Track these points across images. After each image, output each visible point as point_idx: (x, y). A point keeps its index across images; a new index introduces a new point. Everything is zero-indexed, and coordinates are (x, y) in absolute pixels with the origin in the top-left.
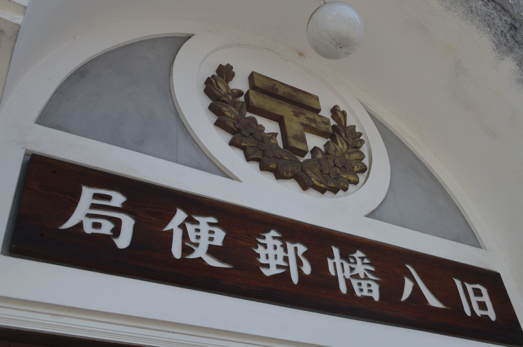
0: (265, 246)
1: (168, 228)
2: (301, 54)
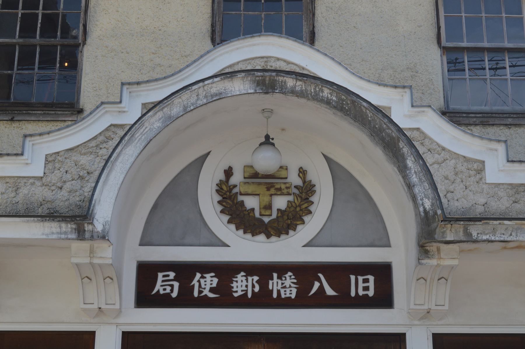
0: (237, 282)
1: (192, 284)
2: (283, 130)
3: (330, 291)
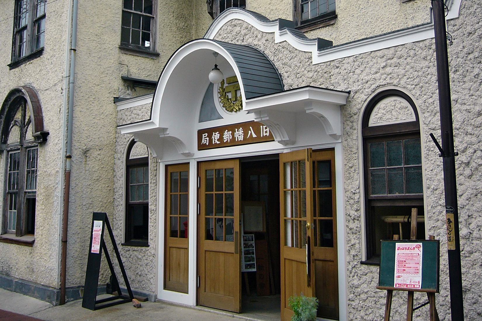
3: (254, 136)
